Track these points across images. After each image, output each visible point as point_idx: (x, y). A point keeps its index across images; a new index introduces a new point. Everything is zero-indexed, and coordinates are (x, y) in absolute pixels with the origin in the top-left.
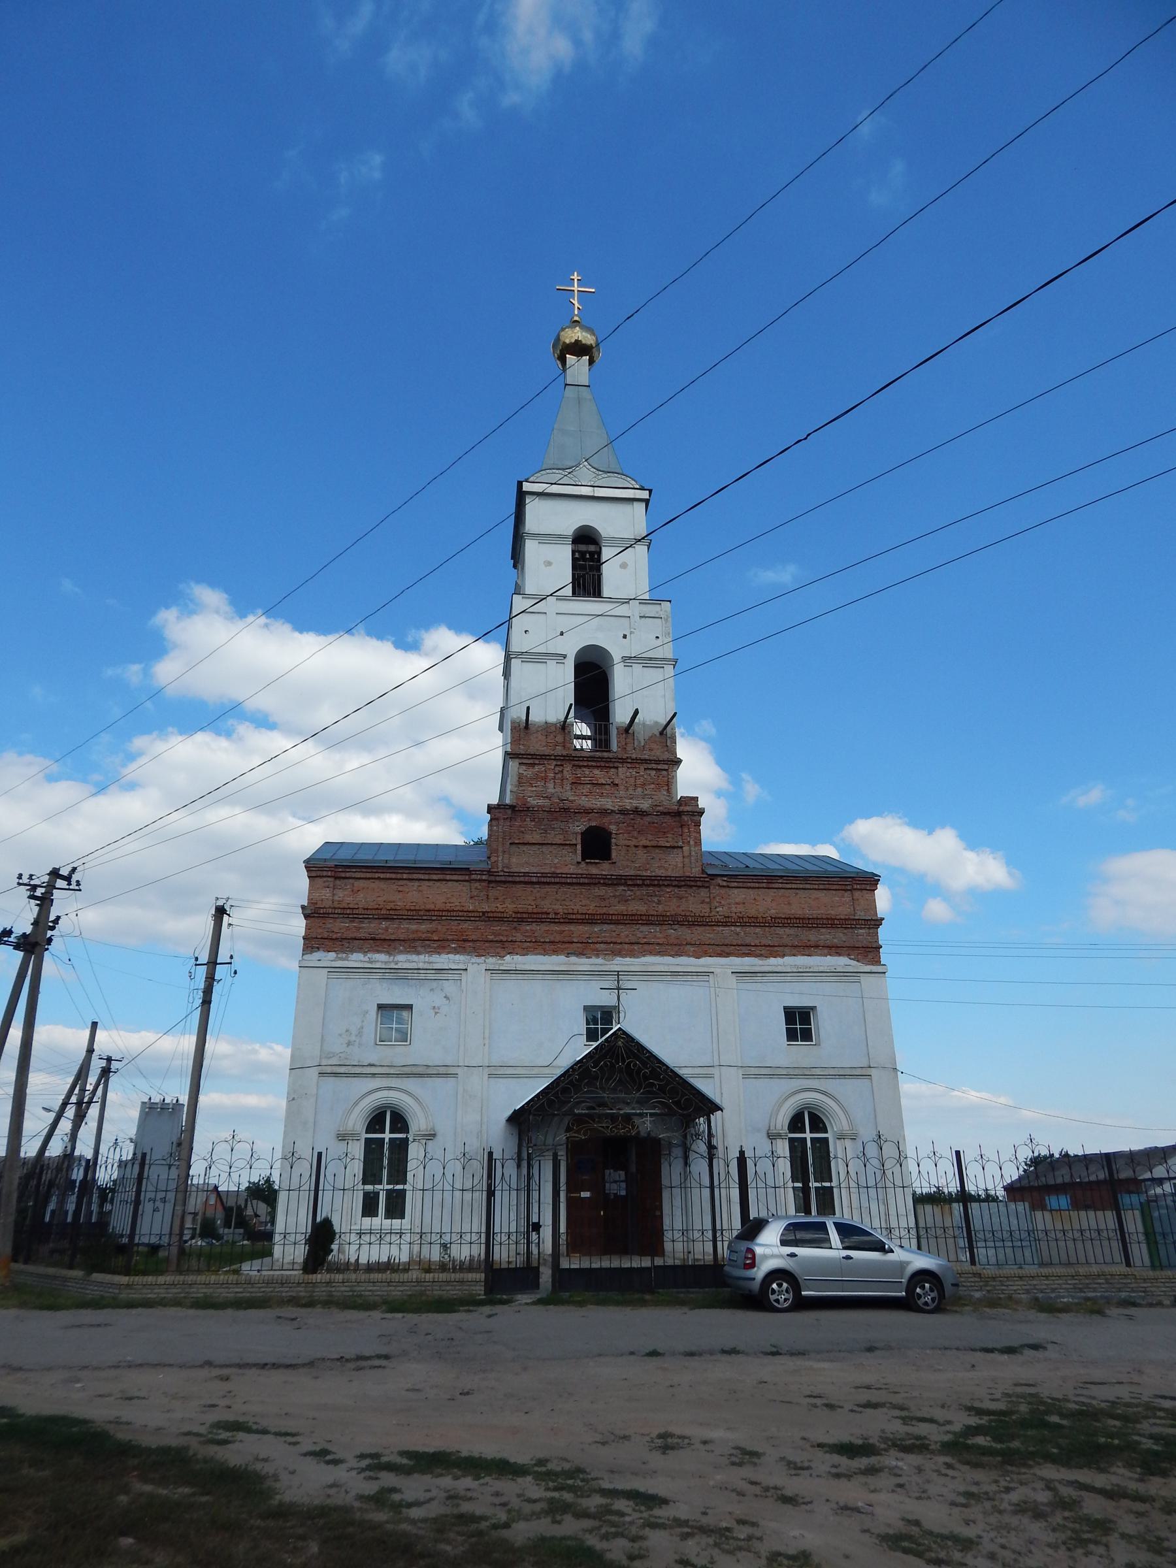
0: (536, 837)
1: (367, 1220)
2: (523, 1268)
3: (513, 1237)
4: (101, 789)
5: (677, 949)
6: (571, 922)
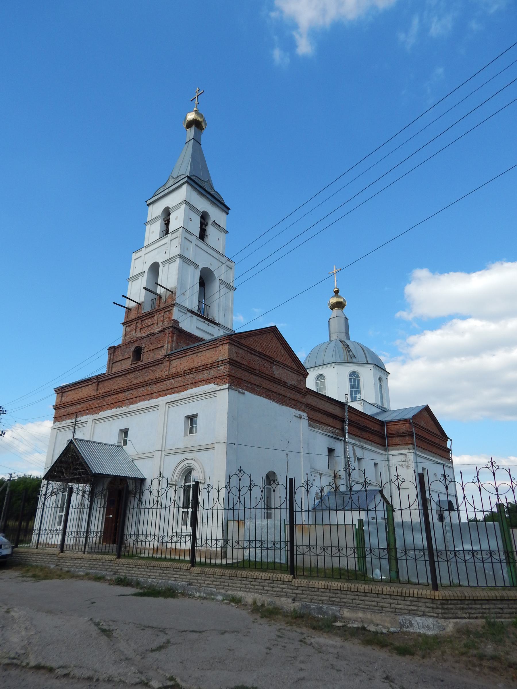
0: (120, 358)
3: (99, 535)
4: (404, 362)
5: (150, 396)
6: (119, 393)
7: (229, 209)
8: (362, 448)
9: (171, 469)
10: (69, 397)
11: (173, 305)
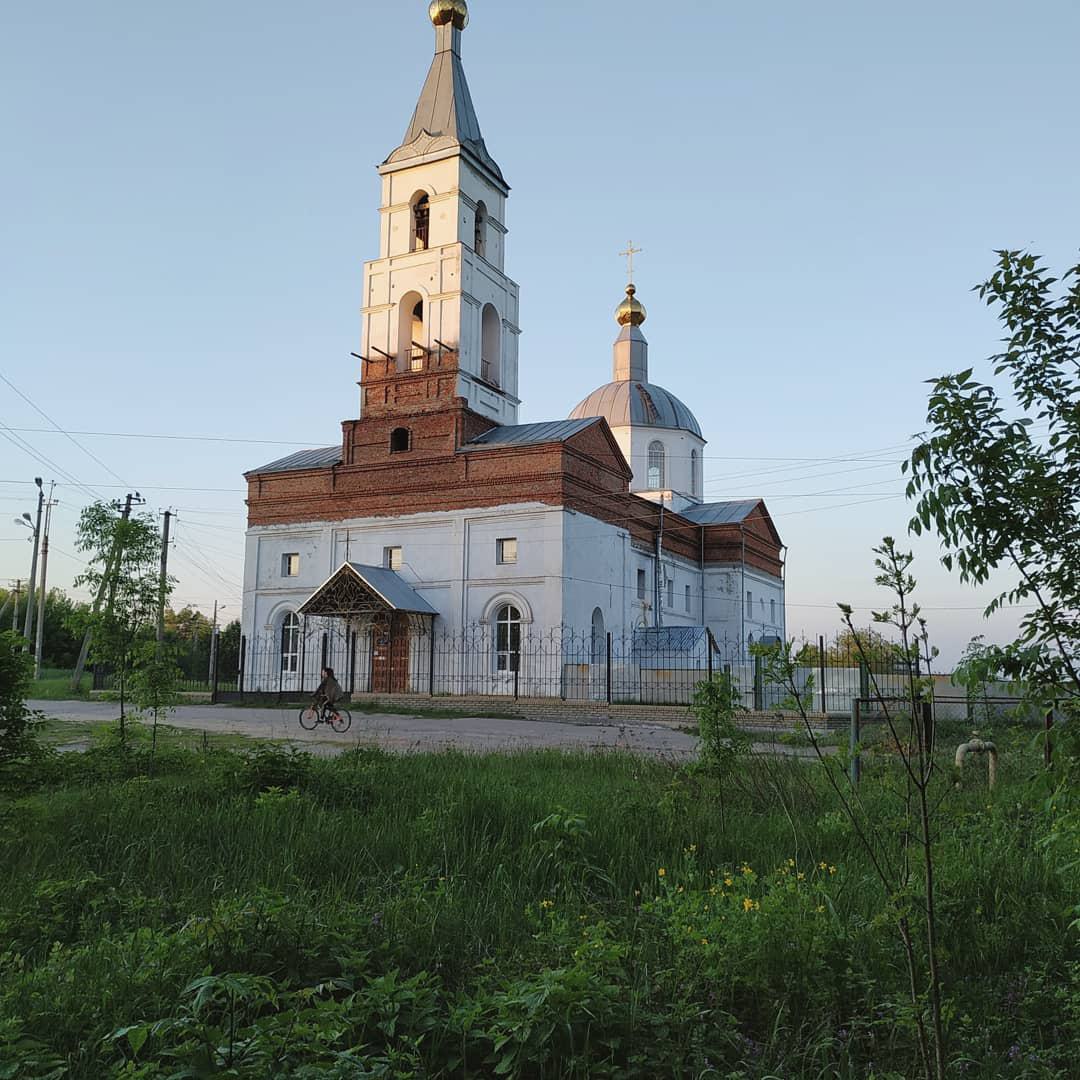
1: (500, 671)
2: (298, 692)
5: (435, 506)
7: (508, 188)
8: (674, 565)
9: (482, 601)
10: (275, 489)
11: (456, 371)
